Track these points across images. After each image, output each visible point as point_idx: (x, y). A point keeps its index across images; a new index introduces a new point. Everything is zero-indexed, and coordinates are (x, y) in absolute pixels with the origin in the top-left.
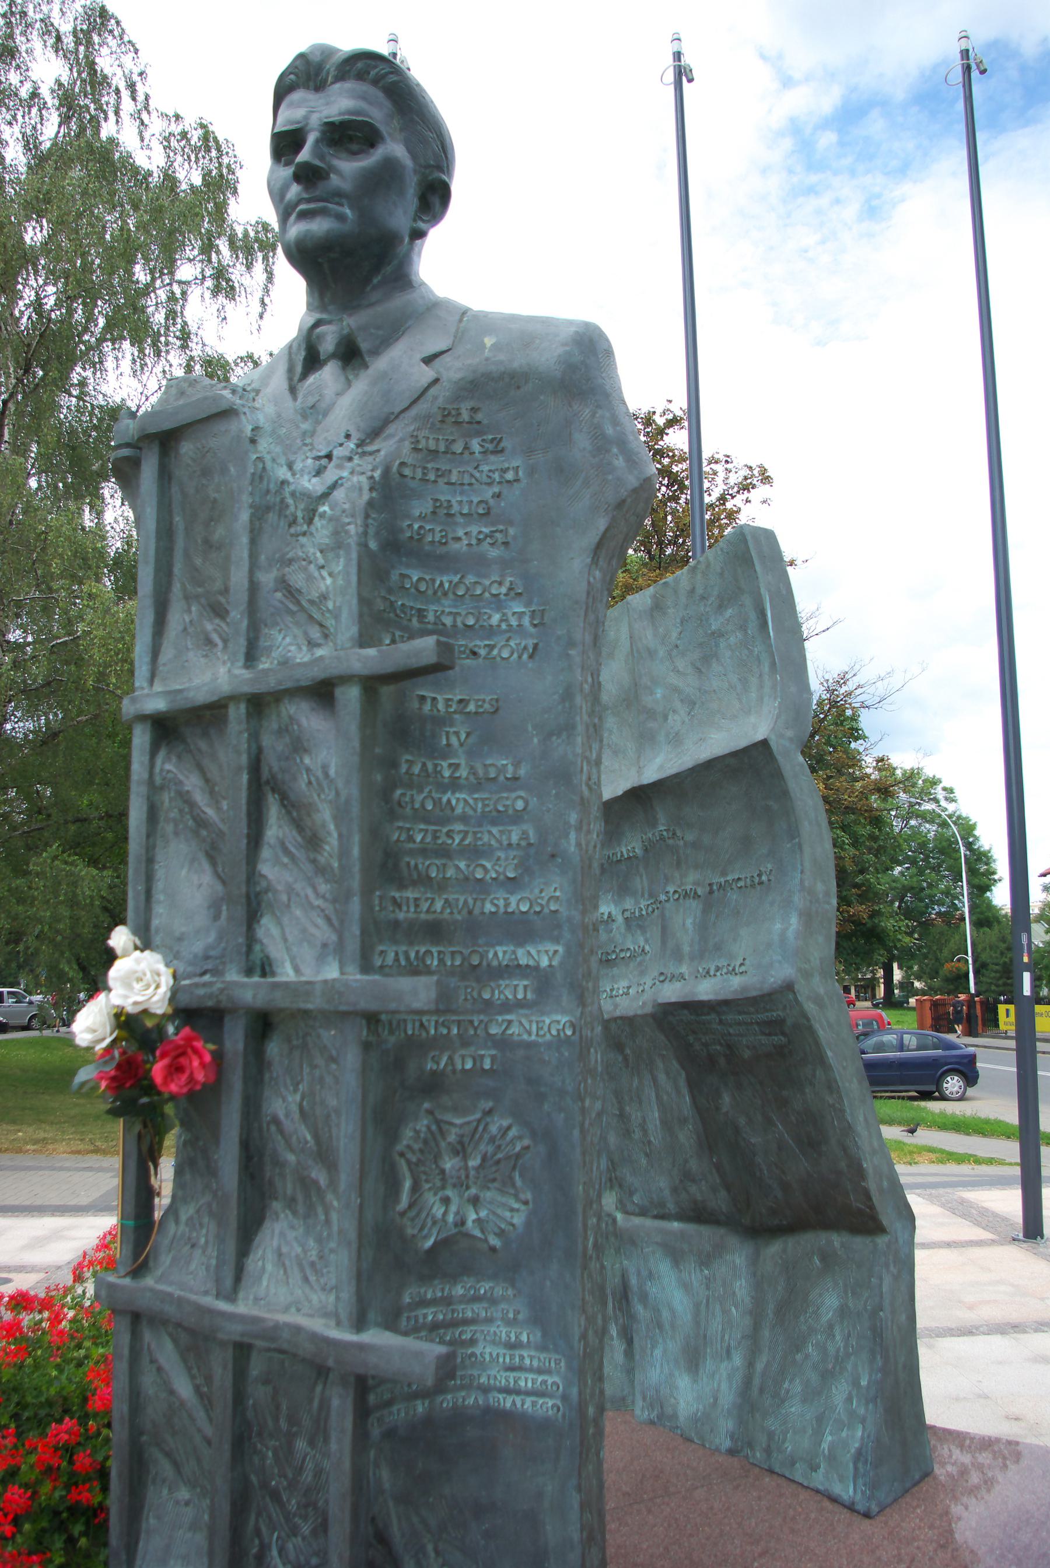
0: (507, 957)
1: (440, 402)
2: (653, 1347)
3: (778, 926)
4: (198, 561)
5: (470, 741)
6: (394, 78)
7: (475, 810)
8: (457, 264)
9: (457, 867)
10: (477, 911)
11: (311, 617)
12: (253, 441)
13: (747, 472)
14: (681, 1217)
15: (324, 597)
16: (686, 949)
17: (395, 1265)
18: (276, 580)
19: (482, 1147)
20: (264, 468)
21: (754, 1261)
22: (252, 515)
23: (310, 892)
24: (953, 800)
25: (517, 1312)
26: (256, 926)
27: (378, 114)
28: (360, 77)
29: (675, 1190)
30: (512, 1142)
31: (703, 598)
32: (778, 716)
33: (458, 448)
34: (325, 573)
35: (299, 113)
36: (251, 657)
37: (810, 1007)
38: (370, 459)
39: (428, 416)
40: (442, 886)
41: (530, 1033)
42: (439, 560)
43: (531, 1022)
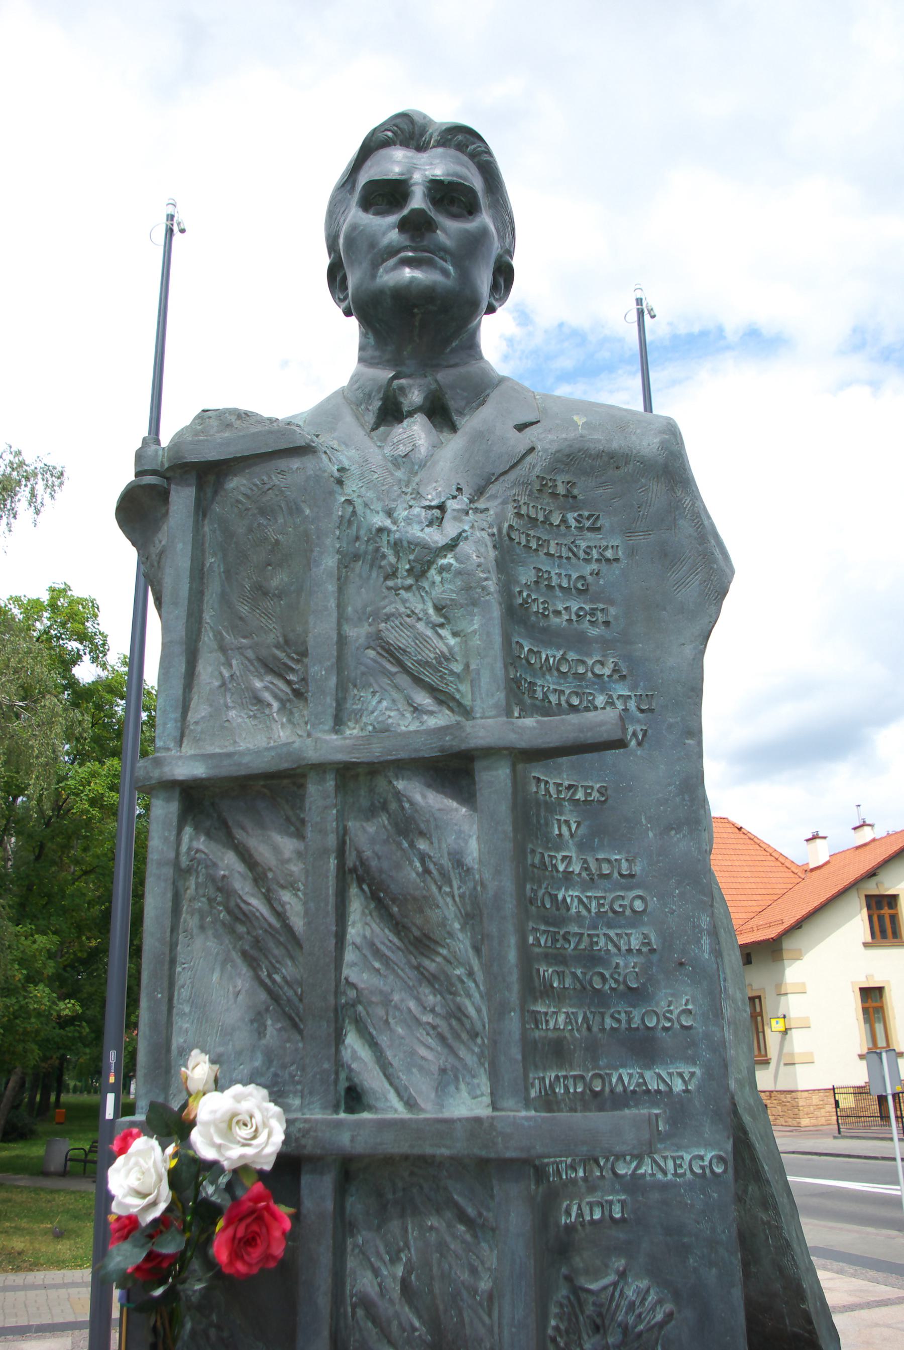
0: (634, 1082)
1: (537, 471)
5: (580, 832)
7: (589, 911)
9: (574, 975)
12: (340, 482)
18: (369, 636)
20: (354, 513)
22: (340, 562)
23: (412, 1004)
26: (342, 1048)
30: (653, 1309)
33: (556, 520)
38: (483, 516)
39: (526, 484)
41: (665, 1173)
43: (665, 1158)
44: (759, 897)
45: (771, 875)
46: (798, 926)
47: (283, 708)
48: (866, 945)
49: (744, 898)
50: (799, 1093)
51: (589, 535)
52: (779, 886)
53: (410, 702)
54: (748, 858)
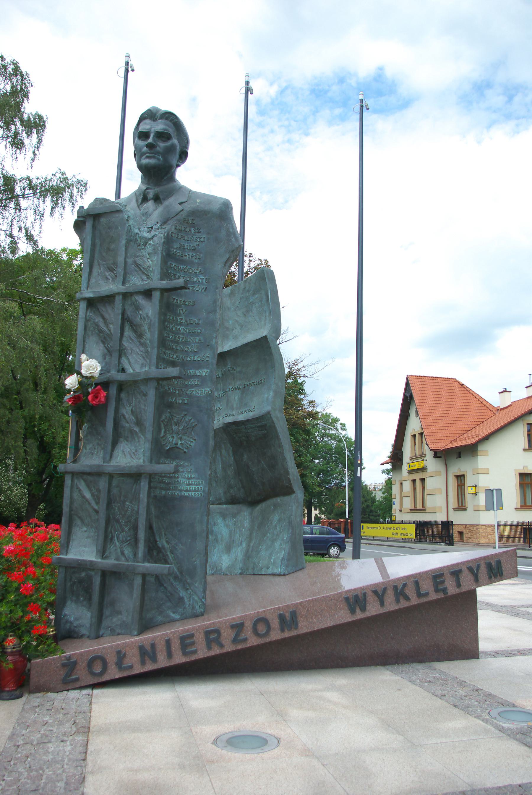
2: (214, 549)
3: (266, 395)
4: (104, 254)
6: (176, 120)
8: (185, 176)
10: (185, 360)
11: (143, 273)
12: (128, 221)
13: (259, 262)
14: (227, 503)
15: (149, 267)
16: (235, 406)
17: (160, 451)
19: (183, 424)
21: (251, 514)
23: (138, 350)
24: (345, 430)
25: (191, 470)
27: (171, 131)
28: (167, 119)
29: (225, 493)
31: (248, 291)
32: (271, 329)
33: (188, 230)
34: (149, 260)
35: (148, 127)
36: (124, 283)
37: (275, 419)
38: (163, 230)
40: (176, 351)
42: (181, 261)
44: (469, 423)
45: (477, 411)
46: (487, 438)
47: (113, 280)
48: (525, 450)
49: (461, 422)
50: (480, 526)
51: (197, 234)
52: (481, 417)
53: (141, 277)
54: (465, 401)
